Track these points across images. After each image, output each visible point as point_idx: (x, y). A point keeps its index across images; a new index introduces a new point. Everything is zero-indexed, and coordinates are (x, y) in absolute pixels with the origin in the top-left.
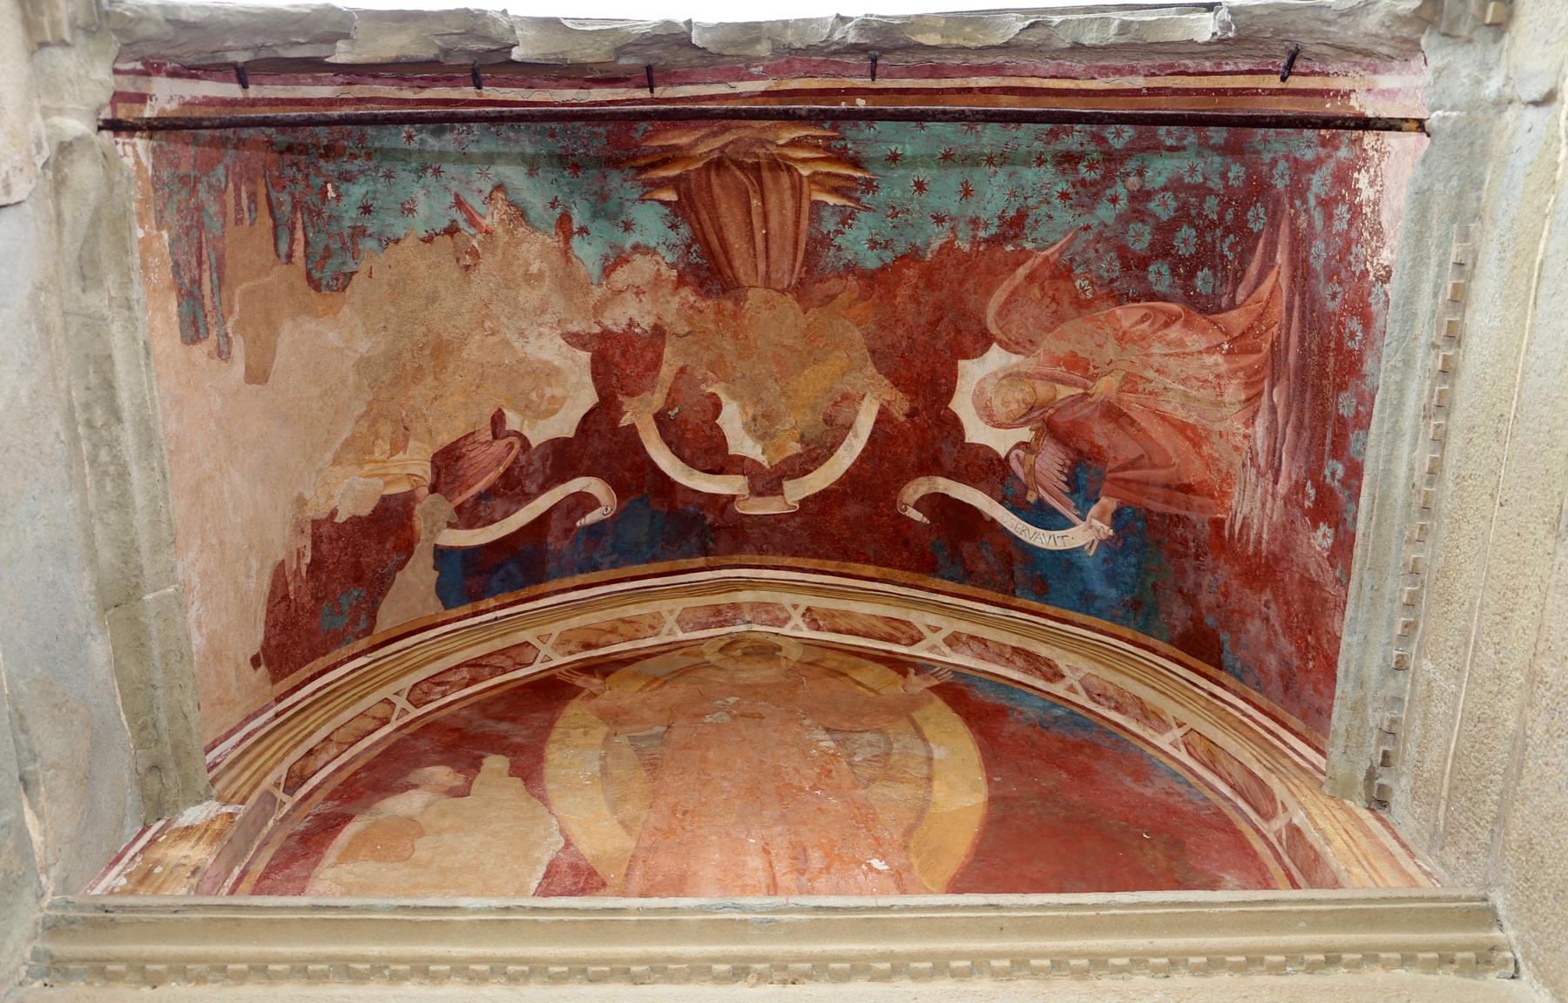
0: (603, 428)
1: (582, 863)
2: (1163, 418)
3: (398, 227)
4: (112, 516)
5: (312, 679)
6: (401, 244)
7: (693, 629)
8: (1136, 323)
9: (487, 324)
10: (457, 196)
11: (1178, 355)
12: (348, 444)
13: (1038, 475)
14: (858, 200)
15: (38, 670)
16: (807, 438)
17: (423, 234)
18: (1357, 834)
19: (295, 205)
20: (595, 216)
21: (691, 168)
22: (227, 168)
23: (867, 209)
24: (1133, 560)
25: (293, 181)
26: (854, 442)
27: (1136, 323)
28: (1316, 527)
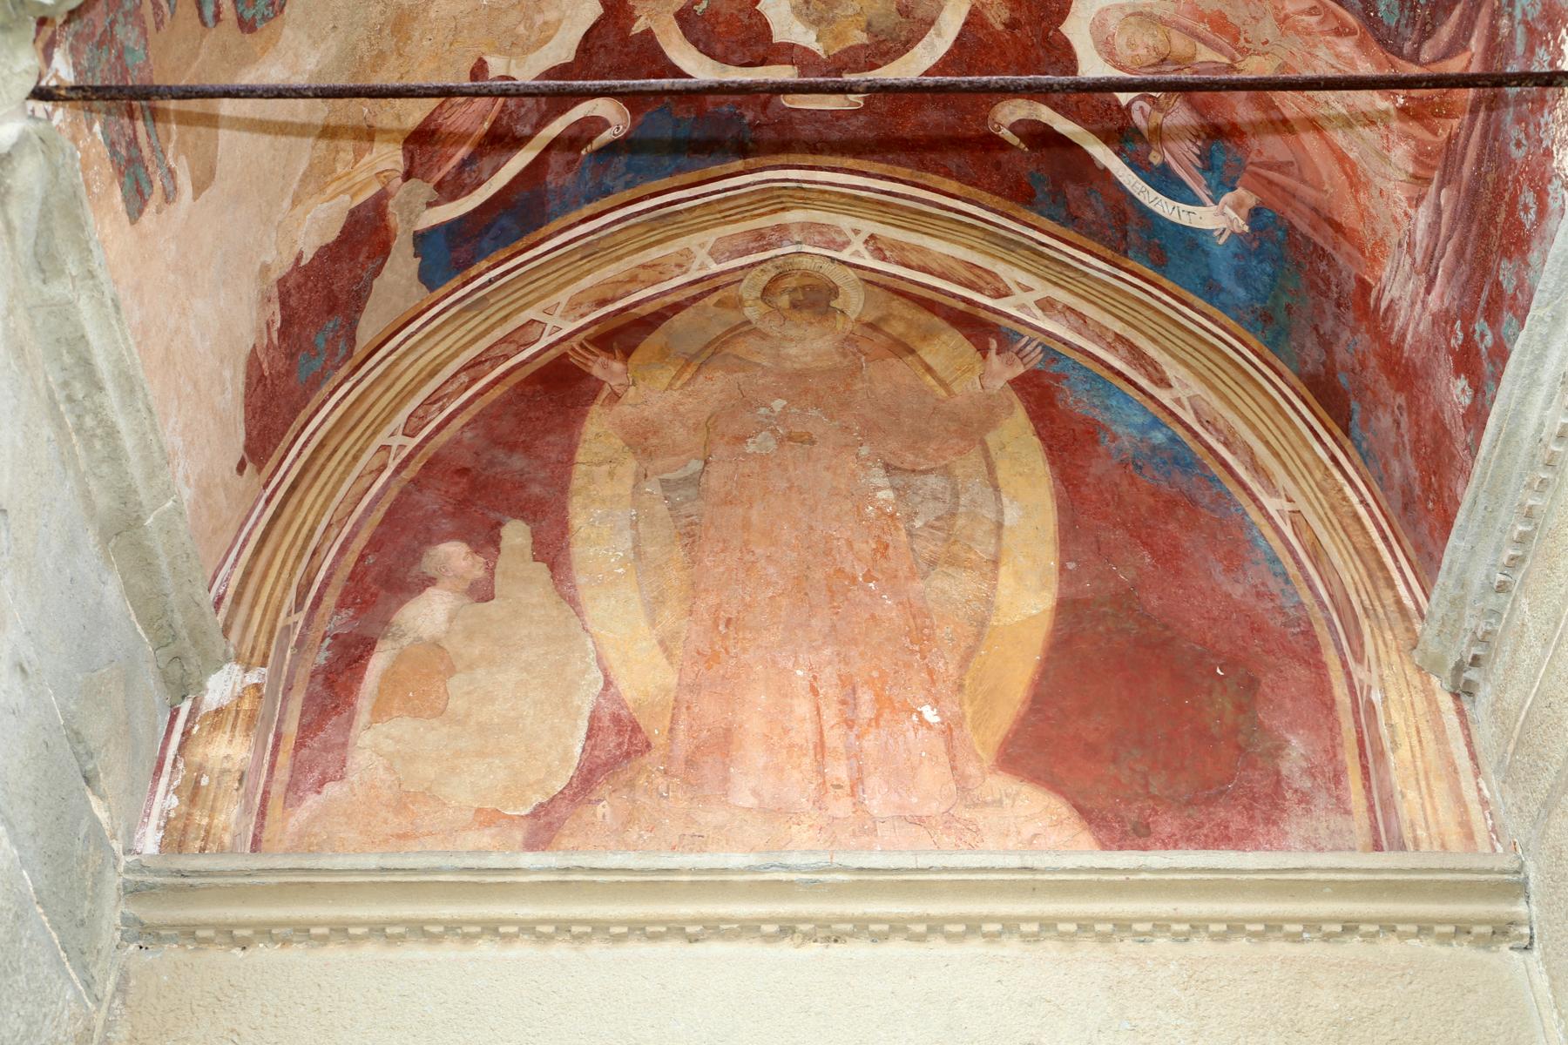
1: (624, 713)
4: (105, 469)
7: (729, 258)
8: (1302, 12)
15: (80, 678)
18: (1428, 736)
26: (937, 41)
27: (1302, 12)
28: (1458, 377)
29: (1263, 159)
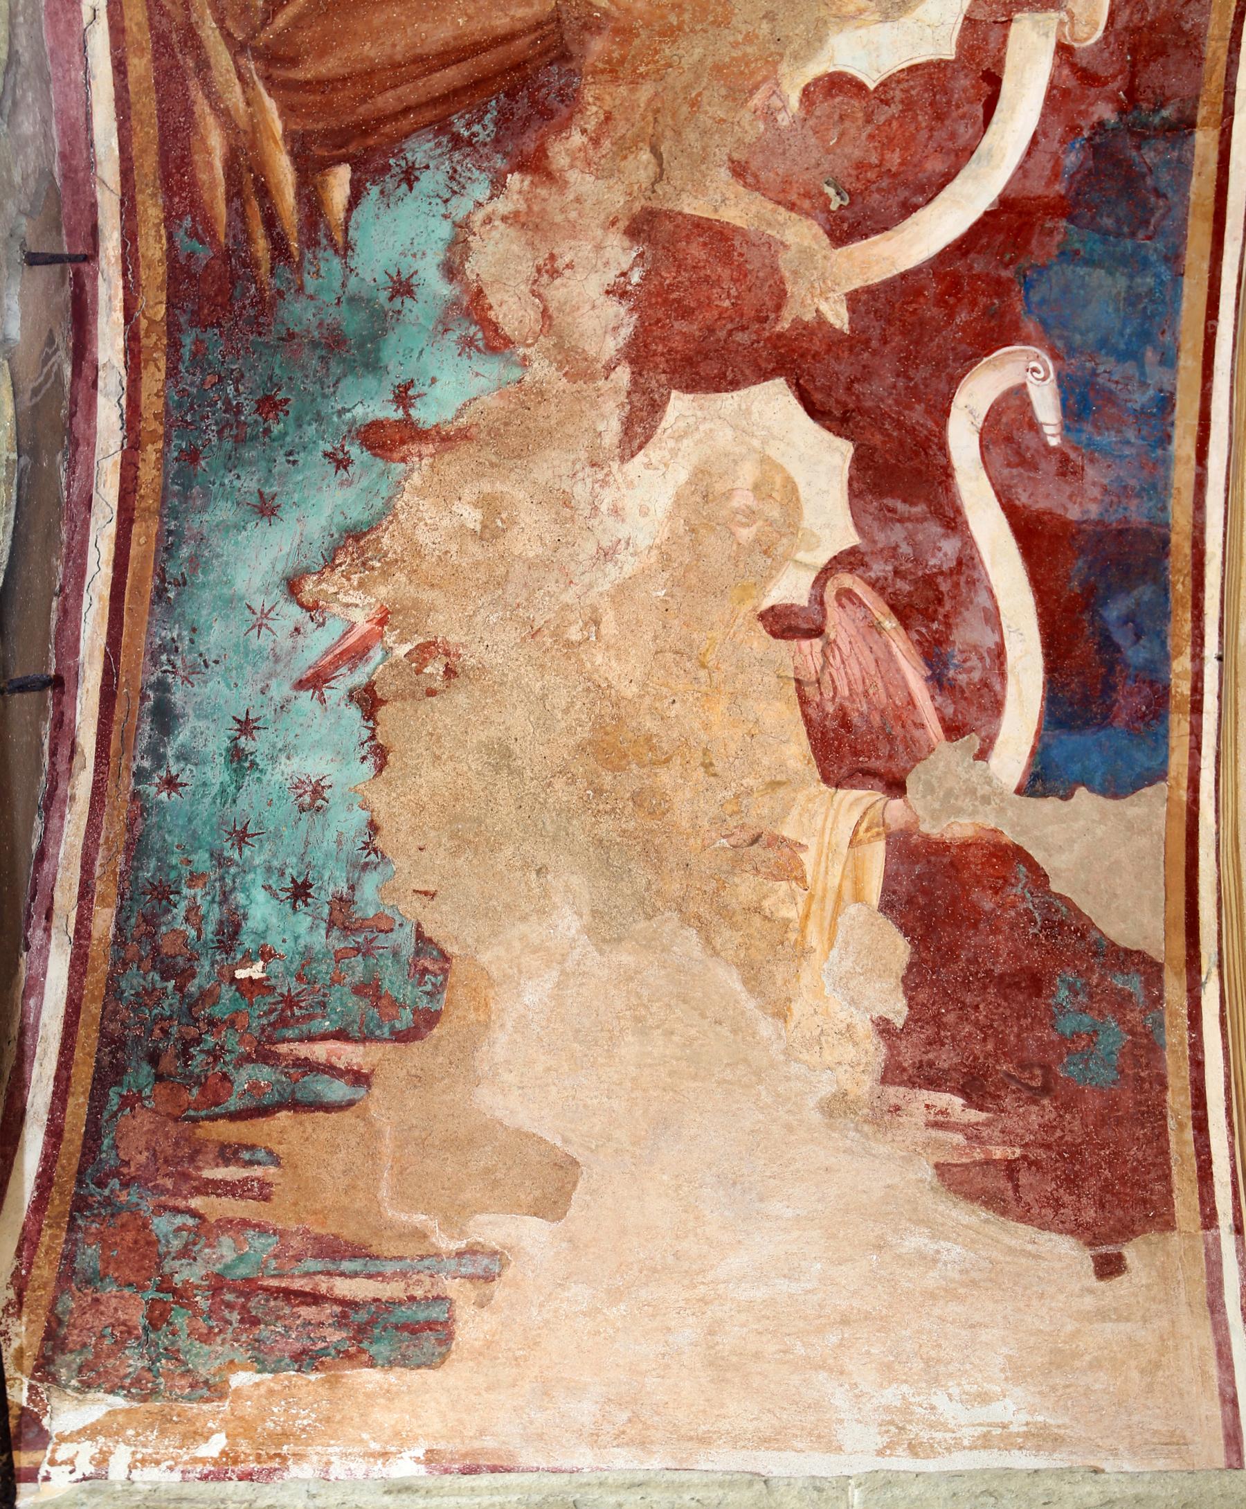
0: (845, 368)
3: (345, 821)
5: (1201, 1126)
6: (380, 820)
9: (574, 634)
10: (301, 685)
12: (753, 977)
17: (368, 768)
19: (265, 1057)
20: (373, 366)
21: (278, 126)
22: (161, 1209)
25: (215, 1055)
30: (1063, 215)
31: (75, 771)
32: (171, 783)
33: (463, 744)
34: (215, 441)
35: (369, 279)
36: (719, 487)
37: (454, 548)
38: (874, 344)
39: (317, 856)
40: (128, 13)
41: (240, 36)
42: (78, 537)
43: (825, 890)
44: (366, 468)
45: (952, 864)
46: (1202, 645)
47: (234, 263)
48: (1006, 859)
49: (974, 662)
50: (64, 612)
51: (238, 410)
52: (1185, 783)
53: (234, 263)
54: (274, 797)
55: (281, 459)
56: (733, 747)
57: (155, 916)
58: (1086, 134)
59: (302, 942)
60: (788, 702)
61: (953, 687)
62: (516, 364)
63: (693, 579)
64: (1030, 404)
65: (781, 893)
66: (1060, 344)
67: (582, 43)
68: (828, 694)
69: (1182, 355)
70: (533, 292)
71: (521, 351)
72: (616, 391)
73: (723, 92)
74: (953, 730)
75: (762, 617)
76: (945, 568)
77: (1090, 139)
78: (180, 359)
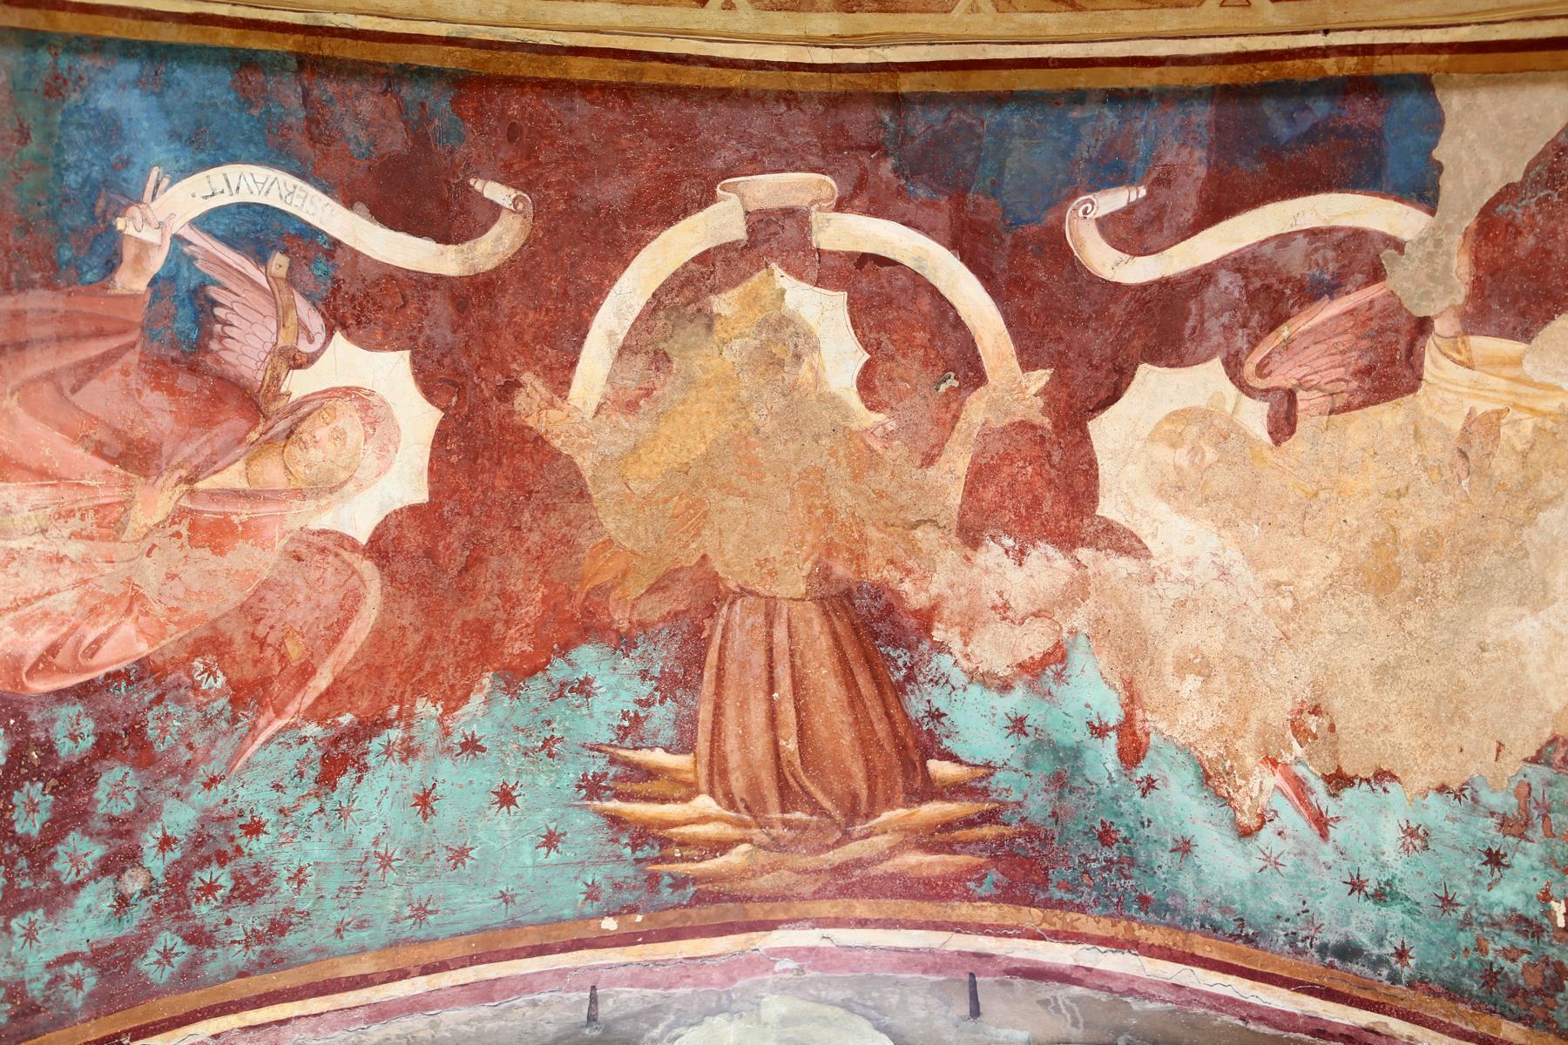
0: (1081, 372)
2: (42, 474)
3: (1437, 812)
8: (107, 635)
9: (1287, 604)
10: (1324, 836)
11: (27, 601)
13: (268, 309)
14: (613, 761)
16: (698, 327)
20: (1076, 753)
21: (901, 812)
23: (597, 748)
24: (72, 179)
26: (613, 323)
27: (107, 635)
29: (118, 366)
30: (964, 196)
31: (1388, 1032)
32: (1402, 954)
33: (1375, 706)
34: (1132, 882)
35: (1012, 751)
36: (1173, 477)
37: (1216, 699)
38: (1062, 348)
39: (1466, 840)
40: (824, 914)
41: (838, 835)
42: (1204, 1000)
43: (1509, 393)
44: (1153, 765)
45: (1492, 275)
46: (1315, 49)
47: (1002, 853)
48: (1491, 225)
49: (1318, 256)
50: (1260, 1019)
51: (1109, 861)
52: (1433, 57)
53: (1002, 853)
54: (1415, 870)
55: (1146, 831)
56: (1384, 472)
57: (1509, 987)
58: (903, 182)
59: (1536, 864)
60: (1348, 422)
61: (1339, 275)
62: (1075, 640)
63: (1245, 501)
64: (1112, 214)
65: (1511, 433)
66: (1065, 192)
67: (838, 581)
68: (1342, 386)
69: (1076, 86)
70: (1021, 624)
71: (1065, 635)
72: (1096, 560)
73: (872, 473)
74: (1376, 274)
75: (1277, 443)
76: (1242, 283)
77: (907, 179)
78: (1071, 902)
